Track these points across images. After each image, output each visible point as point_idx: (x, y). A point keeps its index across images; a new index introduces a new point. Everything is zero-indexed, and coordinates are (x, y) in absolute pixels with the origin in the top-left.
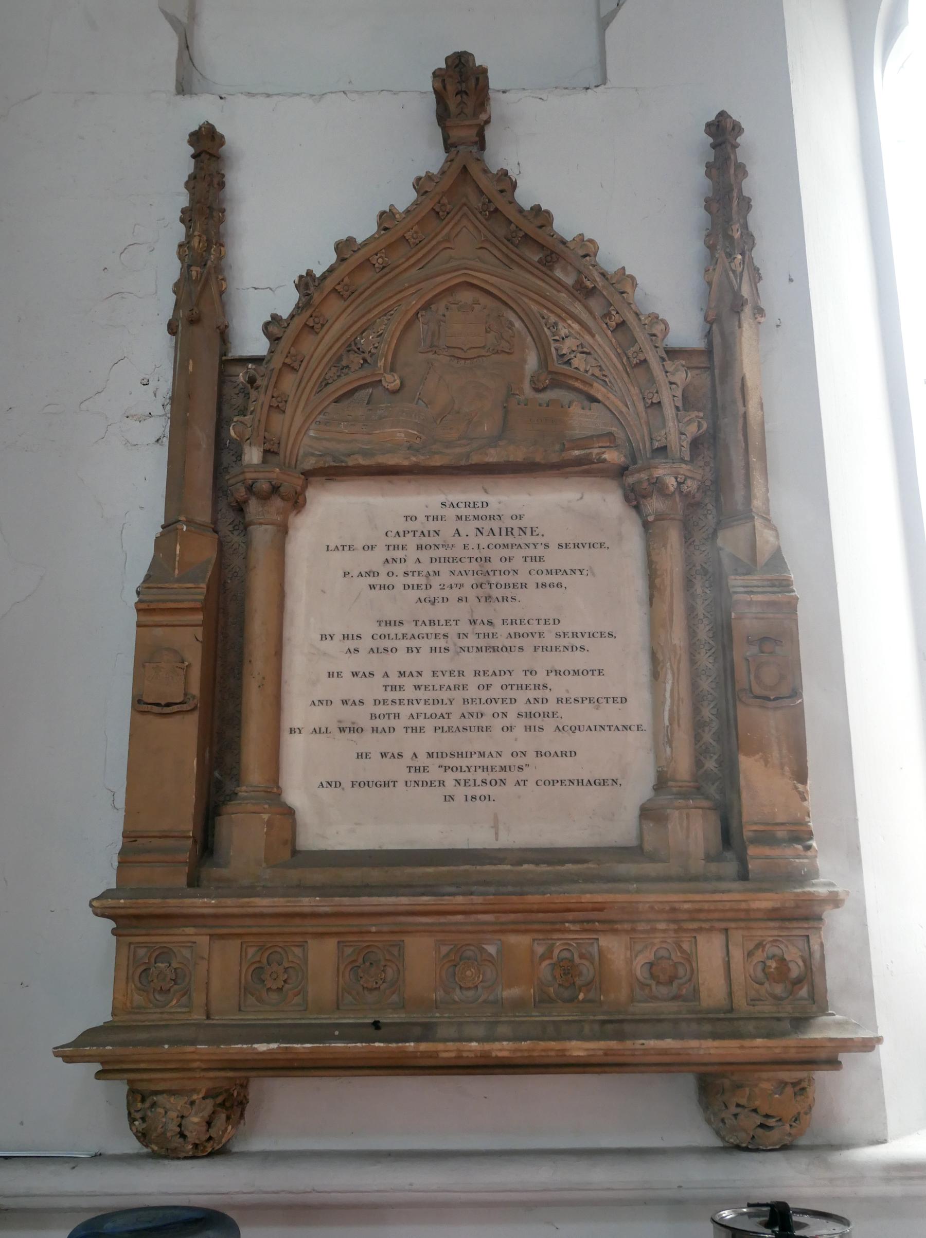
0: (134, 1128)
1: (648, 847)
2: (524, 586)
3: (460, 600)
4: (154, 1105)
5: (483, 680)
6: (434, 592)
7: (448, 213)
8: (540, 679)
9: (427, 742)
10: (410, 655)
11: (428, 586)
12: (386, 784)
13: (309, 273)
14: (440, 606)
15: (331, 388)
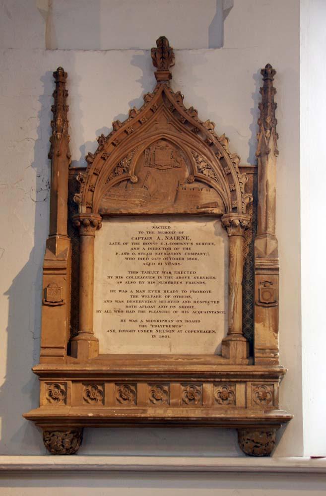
0: (46, 444)
1: (223, 355)
2: (183, 259)
3: (159, 264)
4: (53, 435)
5: (167, 294)
6: (150, 261)
7: (157, 110)
8: (188, 294)
9: (147, 316)
10: (141, 285)
11: (148, 259)
12: (131, 331)
13: (102, 136)
14: (151, 266)
15: (112, 181)
